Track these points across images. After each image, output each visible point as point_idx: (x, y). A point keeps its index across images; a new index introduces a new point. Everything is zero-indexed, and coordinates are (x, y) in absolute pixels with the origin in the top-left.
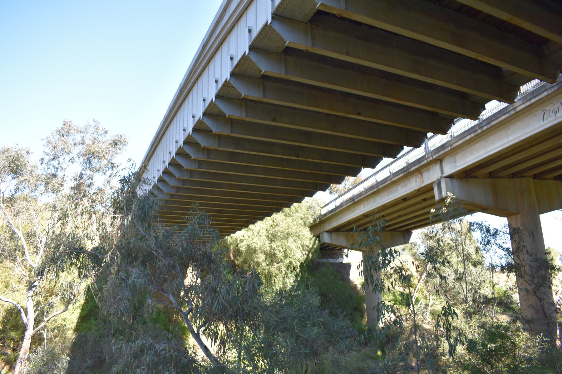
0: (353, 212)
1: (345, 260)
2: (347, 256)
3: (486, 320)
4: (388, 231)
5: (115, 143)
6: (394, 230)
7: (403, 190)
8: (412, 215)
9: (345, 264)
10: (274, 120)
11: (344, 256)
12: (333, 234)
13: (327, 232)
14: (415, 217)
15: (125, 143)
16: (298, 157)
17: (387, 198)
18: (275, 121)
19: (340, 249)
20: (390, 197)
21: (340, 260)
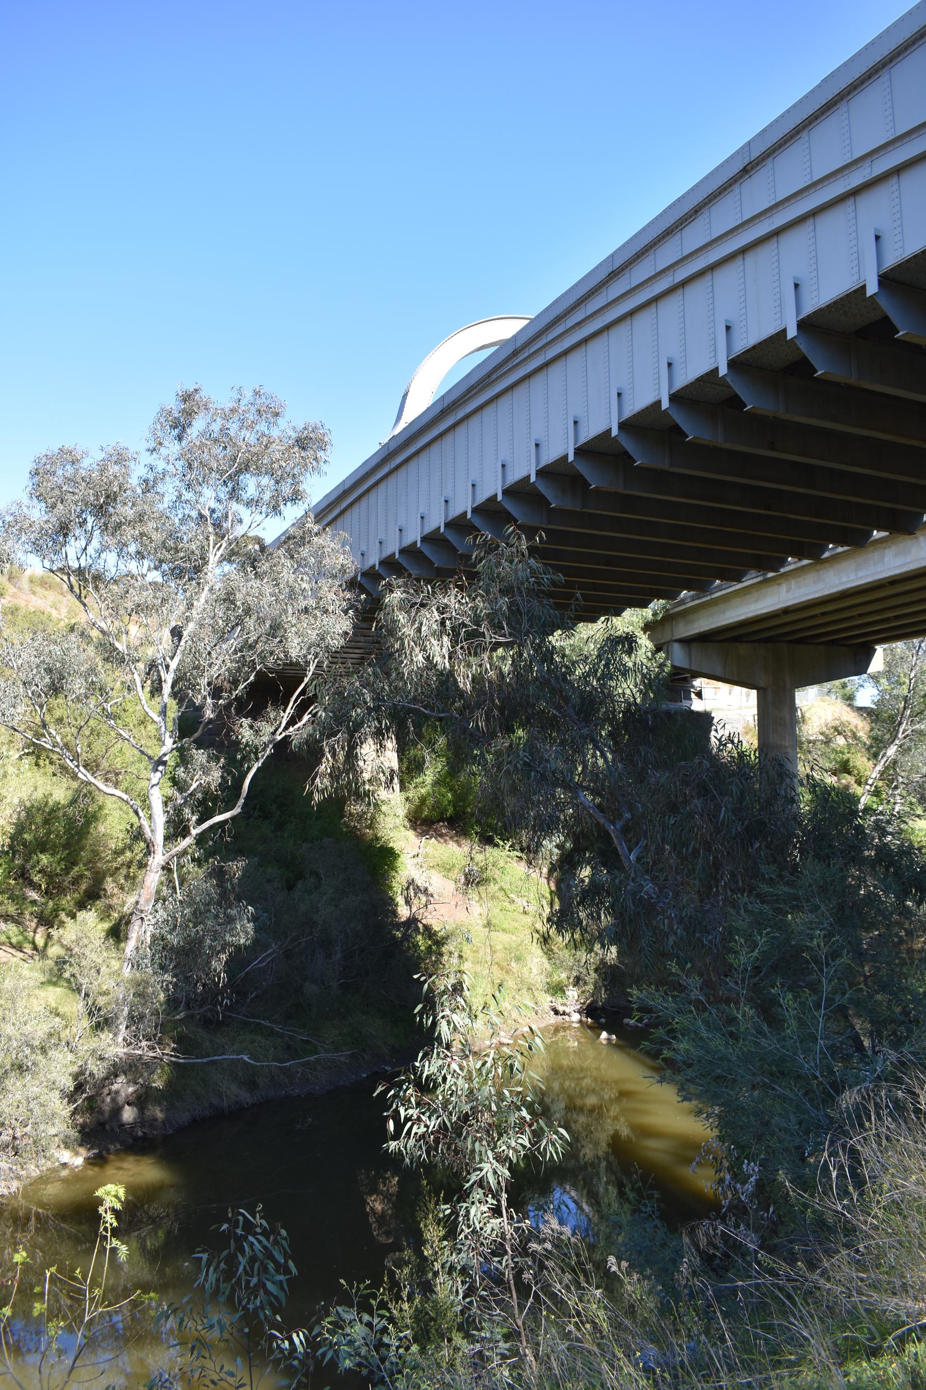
0: (757, 600)
1: (697, 705)
2: (699, 695)
3: (409, 866)
4: (846, 645)
5: (302, 443)
6: (833, 642)
7: (899, 561)
8: (891, 614)
9: (698, 714)
10: (772, 446)
11: (693, 696)
12: (694, 646)
13: (680, 641)
14: (897, 617)
15: (322, 444)
16: (769, 510)
17: (852, 576)
18: (773, 449)
19: (685, 679)
20: (860, 574)
21: (685, 703)
